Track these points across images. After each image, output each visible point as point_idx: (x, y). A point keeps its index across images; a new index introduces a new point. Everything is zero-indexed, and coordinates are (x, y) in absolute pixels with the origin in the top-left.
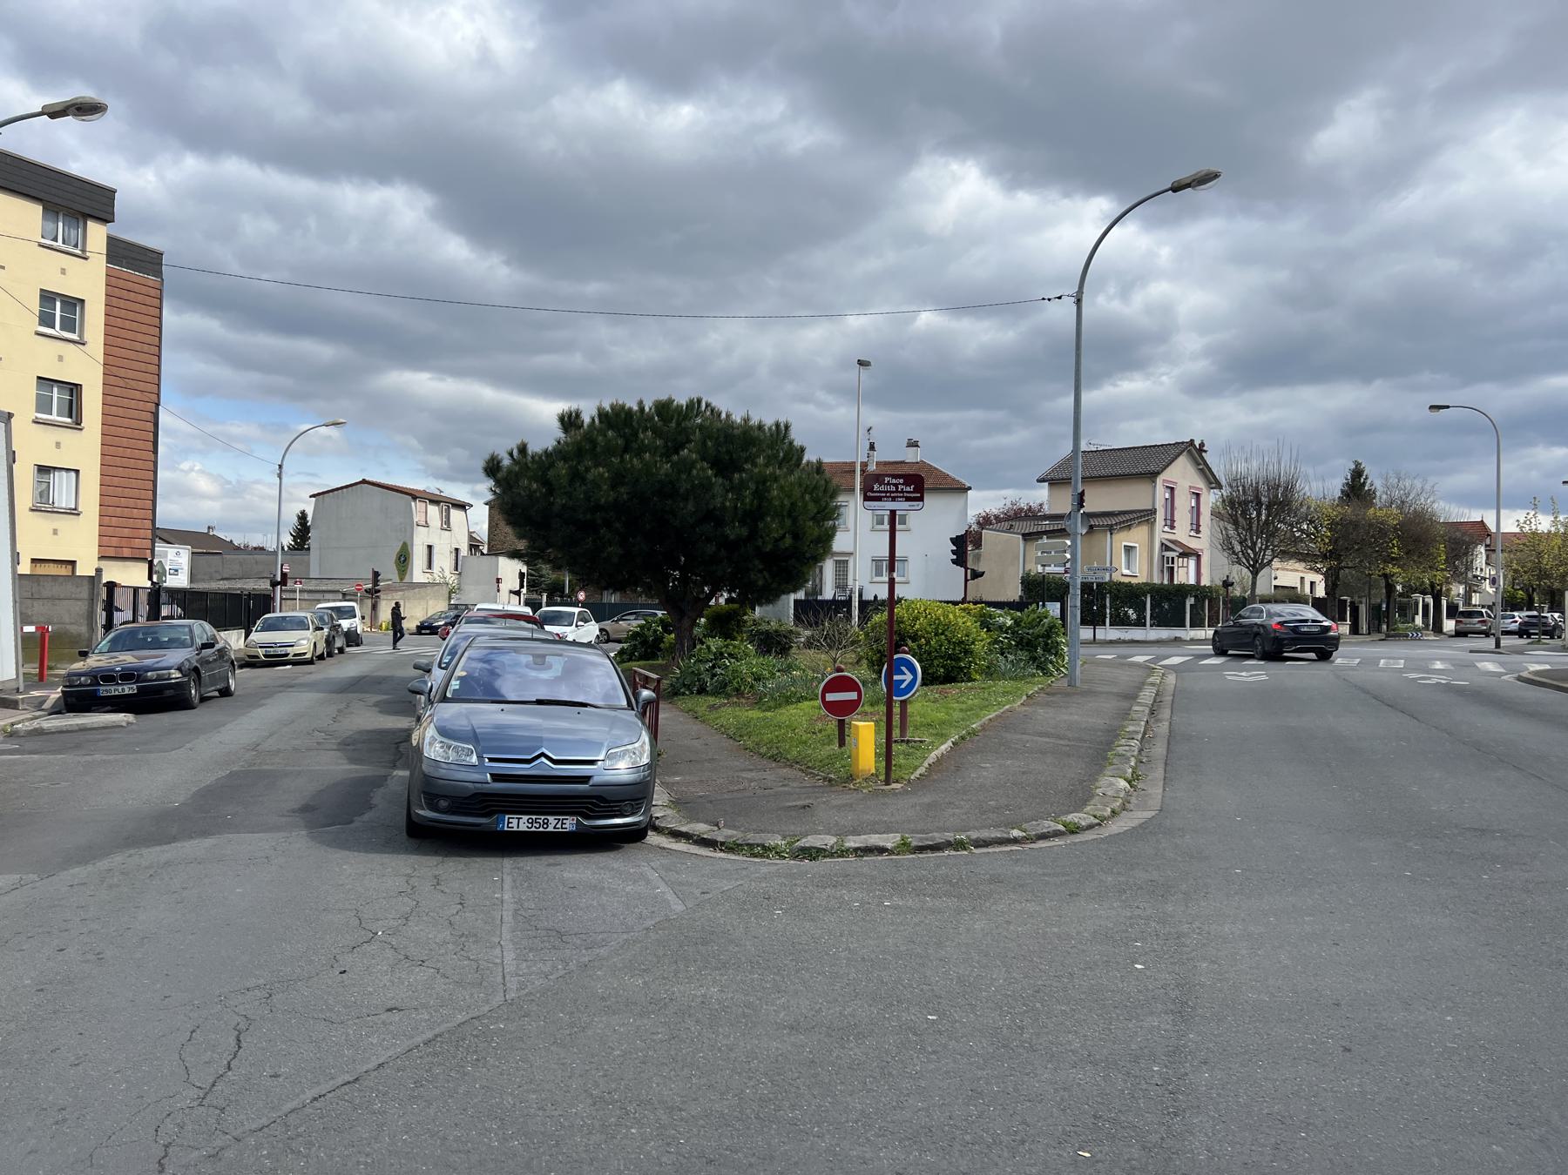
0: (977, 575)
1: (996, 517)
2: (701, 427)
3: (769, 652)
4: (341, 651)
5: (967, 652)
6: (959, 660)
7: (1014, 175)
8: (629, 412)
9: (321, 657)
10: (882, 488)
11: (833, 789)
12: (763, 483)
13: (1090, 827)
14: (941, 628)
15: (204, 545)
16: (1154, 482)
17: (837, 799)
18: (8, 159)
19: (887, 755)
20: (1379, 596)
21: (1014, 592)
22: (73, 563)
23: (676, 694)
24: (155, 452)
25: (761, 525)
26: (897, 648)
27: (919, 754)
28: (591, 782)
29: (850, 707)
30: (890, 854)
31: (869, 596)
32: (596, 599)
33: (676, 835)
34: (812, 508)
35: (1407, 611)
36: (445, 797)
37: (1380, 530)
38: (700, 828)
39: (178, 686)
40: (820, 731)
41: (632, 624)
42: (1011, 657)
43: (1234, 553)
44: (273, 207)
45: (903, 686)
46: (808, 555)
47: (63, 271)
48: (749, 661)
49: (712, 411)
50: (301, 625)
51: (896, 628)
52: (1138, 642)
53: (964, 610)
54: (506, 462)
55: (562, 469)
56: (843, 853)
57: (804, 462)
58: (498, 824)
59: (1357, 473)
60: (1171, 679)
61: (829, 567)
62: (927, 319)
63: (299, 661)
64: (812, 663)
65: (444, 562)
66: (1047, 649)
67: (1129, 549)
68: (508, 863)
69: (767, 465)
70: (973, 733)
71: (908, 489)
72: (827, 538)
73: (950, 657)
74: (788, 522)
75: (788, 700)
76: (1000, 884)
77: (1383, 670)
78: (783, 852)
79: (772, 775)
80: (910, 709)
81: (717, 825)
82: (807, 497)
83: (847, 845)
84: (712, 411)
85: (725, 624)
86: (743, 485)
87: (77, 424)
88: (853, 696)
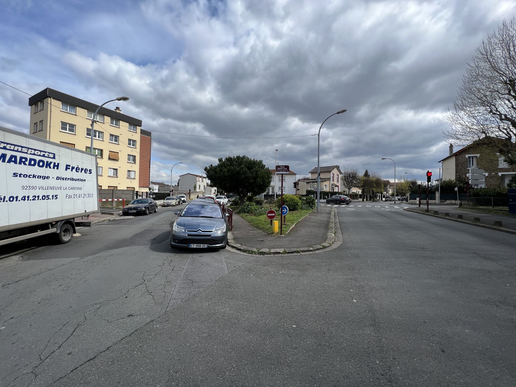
0: (298, 190)
1: (301, 180)
2: (245, 161)
3: (258, 205)
4: (182, 204)
5: (297, 205)
6: (296, 206)
7: (304, 120)
8: (232, 158)
9: (177, 205)
10: (280, 169)
11: (269, 236)
12: (257, 171)
13: (328, 246)
14: (292, 200)
15: (161, 185)
16: (330, 173)
17: (270, 238)
18: (122, 115)
19: (281, 228)
20: (371, 194)
21: (305, 193)
22: (117, 187)
23: (240, 213)
24: (150, 168)
25: (257, 180)
26: (283, 204)
27: (288, 227)
28: (211, 236)
29: (273, 217)
30: (281, 254)
31: (278, 194)
32: (228, 194)
33: (233, 247)
34: (267, 177)
35: (376, 197)
36: (178, 240)
37: (372, 182)
38: (238, 246)
39: (144, 211)
40: (267, 222)
41: (233, 199)
42: (306, 205)
43: (345, 186)
44: (176, 127)
45: (284, 212)
46: (266, 186)
47: (133, 135)
48: (254, 206)
49: (247, 158)
50: (173, 199)
51: (283, 200)
52: (114, 159)
53: (296, 196)
54: (208, 168)
55: (218, 169)
56: (270, 253)
57: (265, 168)
58: (189, 246)
59: (367, 172)
60: (336, 209)
61: (271, 189)
62: (289, 145)
63: (173, 206)
64: (266, 206)
65: (202, 188)
66: (313, 204)
67: (326, 185)
68: (191, 255)
69: (258, 168)
70: (299, 222)
71: (286, 169)
72: (269, 182)
73: (294, 206)
74: (262, 179)
75: (261, 215)
76: (309, 265)
77: (376, 208)
78: (256, 253)
79: (256, 232)
80: (286, 217)
81: (242, 245)
82: (266, 174)
83: (271, 251)
84: (247, 158)
85: (250, 199)
86: (253, 172)
87: (135, 163)
88: (274, 214)
